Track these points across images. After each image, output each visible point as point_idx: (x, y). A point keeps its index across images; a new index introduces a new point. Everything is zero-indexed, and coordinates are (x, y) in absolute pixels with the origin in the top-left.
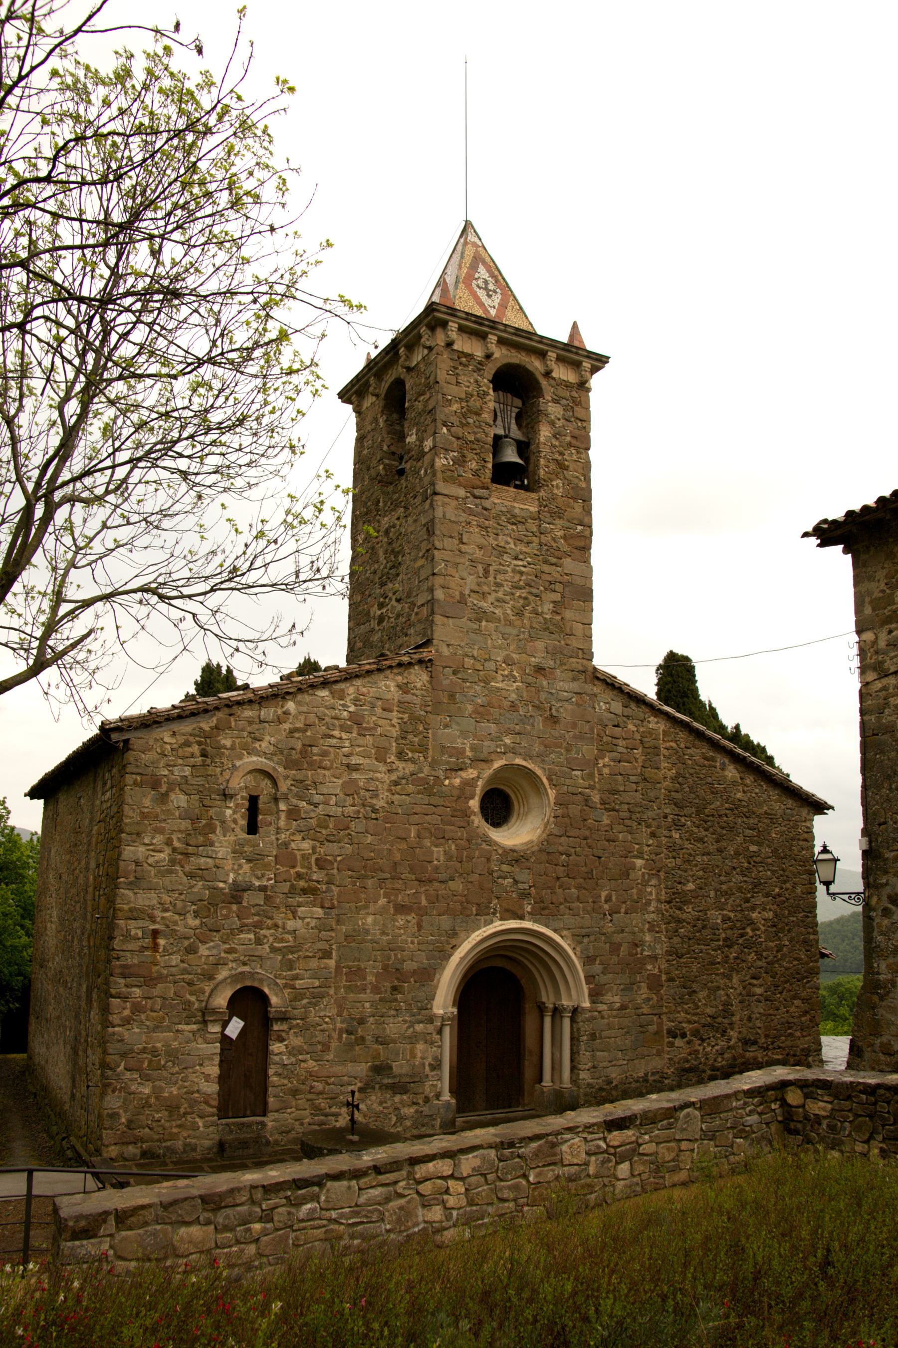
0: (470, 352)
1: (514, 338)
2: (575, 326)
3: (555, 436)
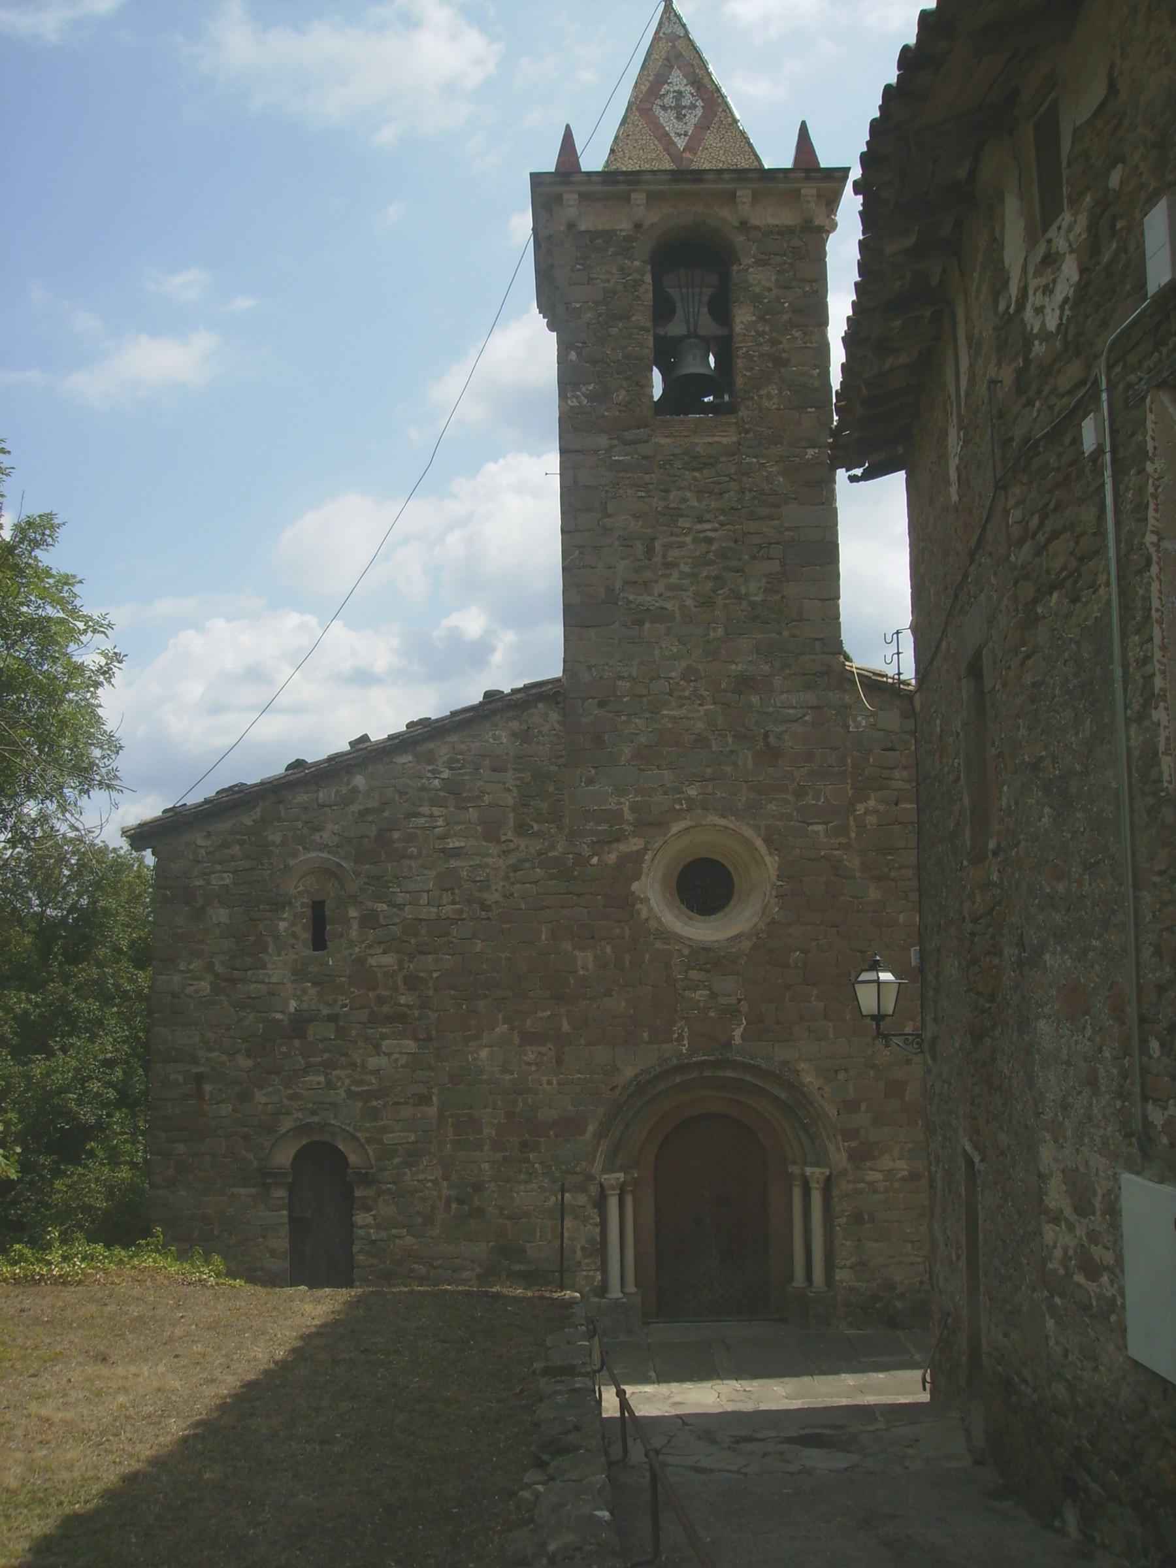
3: (761, 318)
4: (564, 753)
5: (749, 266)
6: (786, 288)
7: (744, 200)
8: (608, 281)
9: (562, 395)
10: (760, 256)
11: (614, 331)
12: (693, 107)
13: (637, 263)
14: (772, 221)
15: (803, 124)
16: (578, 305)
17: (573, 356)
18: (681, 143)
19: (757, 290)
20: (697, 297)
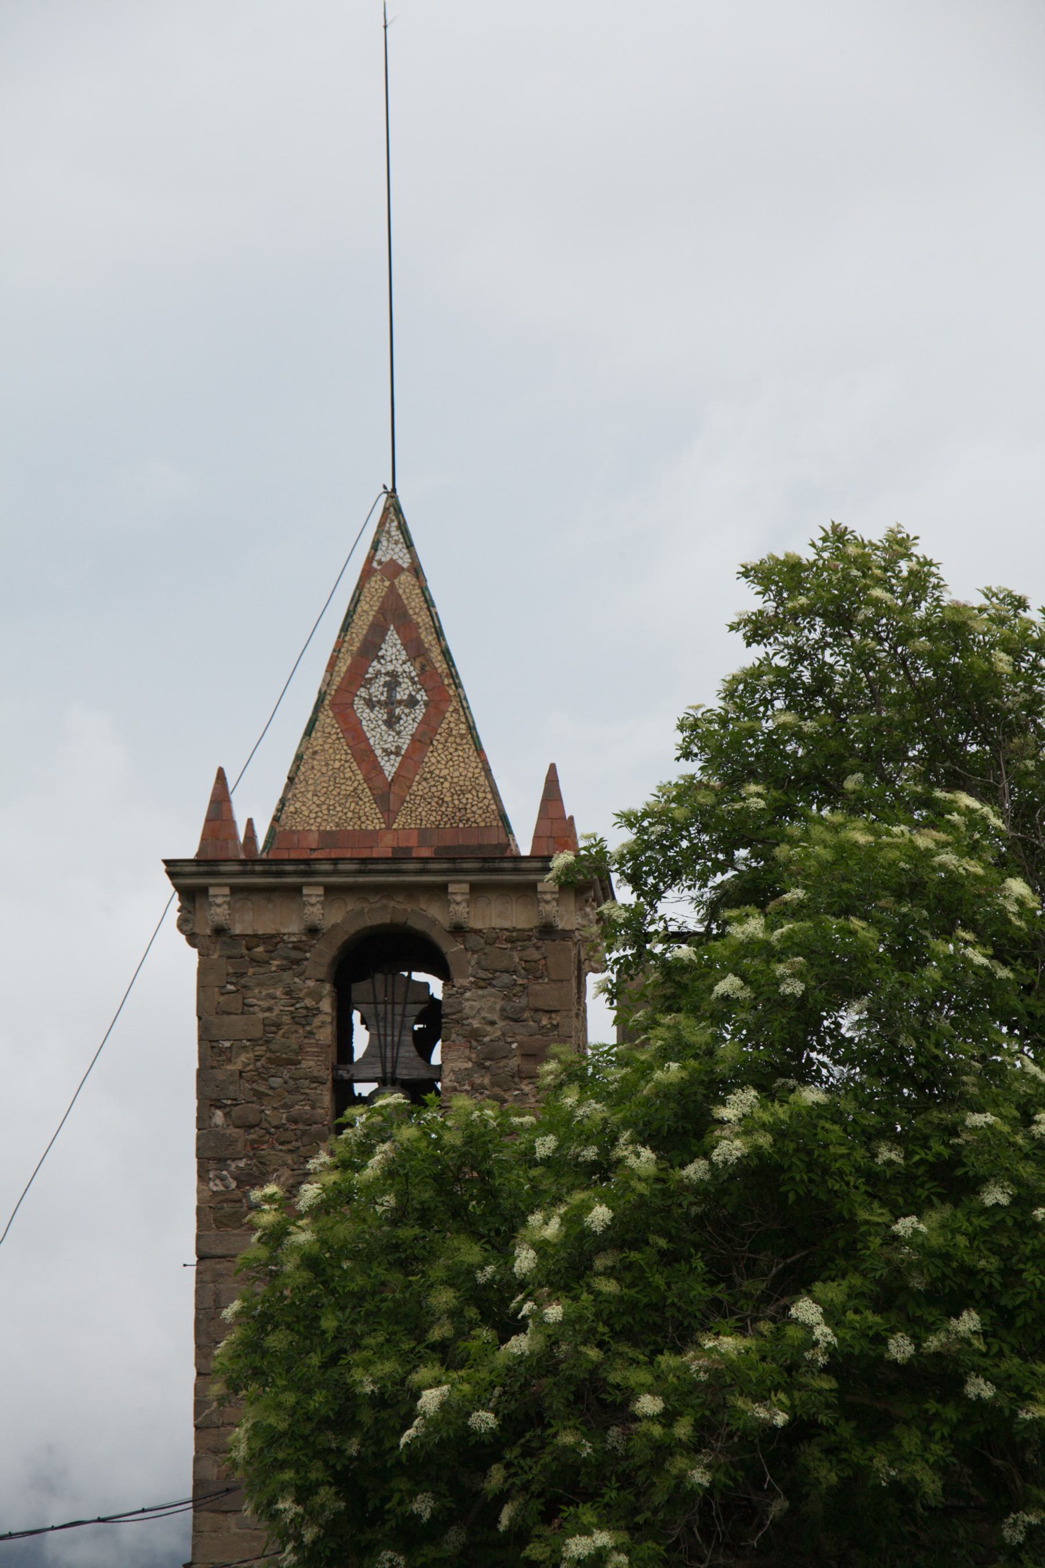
0: (270, 931)
1: (360, 879)
2: (553, 768)
3: (480, 1065)
4: (858, 1326)
5: (466, 989)
6: (516, 1021)
7: (458, 898)
8: (270, 1009)
9: (203, 1175)
10: (482, 974)
11: (276, 1082)
12: (412, 702)
13: (311, 983)
14: (498, 923)
15: (553, 768)
16: (227, 1044)
17: (219, 1117)
18: (390, 767)
19: (476, 1024)
20: (398, 1018)
